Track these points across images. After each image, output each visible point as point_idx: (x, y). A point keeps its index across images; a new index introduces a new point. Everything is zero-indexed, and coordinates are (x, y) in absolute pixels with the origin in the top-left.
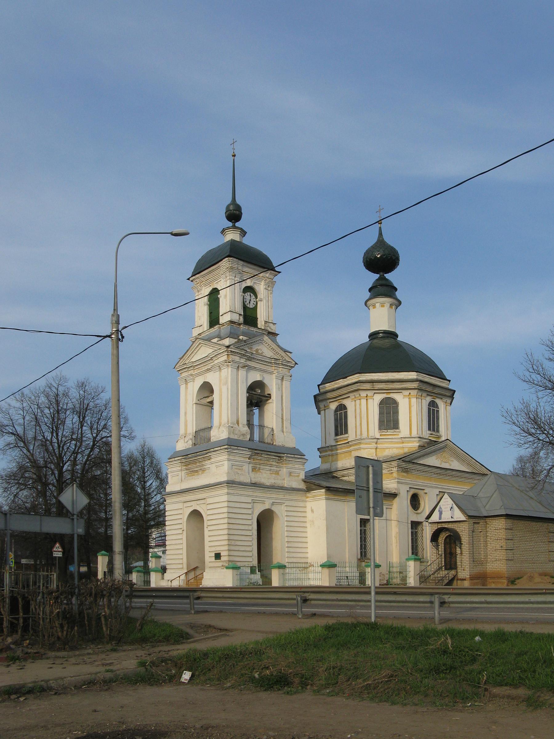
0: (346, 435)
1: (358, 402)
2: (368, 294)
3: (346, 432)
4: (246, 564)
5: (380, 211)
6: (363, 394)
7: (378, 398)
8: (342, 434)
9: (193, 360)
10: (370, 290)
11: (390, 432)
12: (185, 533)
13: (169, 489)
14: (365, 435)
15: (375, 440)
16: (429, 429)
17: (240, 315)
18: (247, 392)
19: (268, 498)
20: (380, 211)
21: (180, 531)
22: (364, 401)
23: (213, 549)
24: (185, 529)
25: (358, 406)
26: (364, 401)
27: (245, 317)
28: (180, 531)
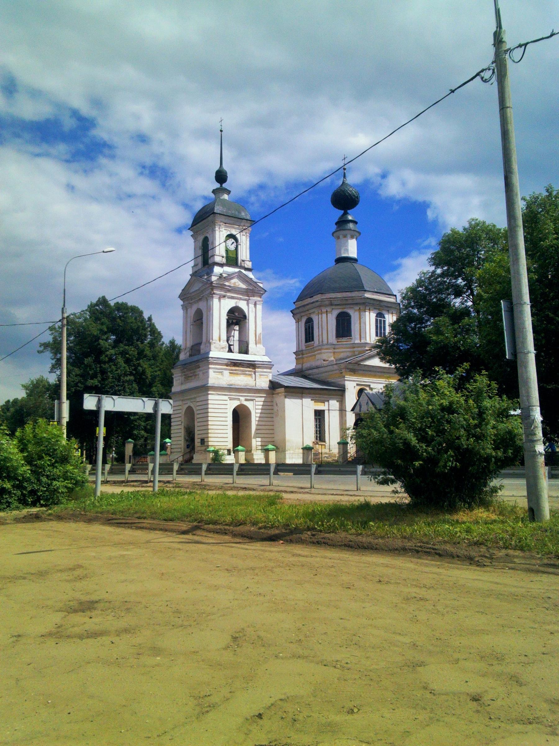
0: (313, 342)
1: (320, 316)
2: (334, 227)
3: (313, 340)
4: (223, 447)
5: (345, 159)
6: (324, 310)
7: (336, 313)
8: (310, 341)
9: (191, 291)
10: (336, 224)
11: (344, 339)
12: (183, 424)
13: (174, 389)
14: (325, 342)
15: (333, 346)
16: (377, 335)
17: (223, 257)
18: (227, 315)
19: (241, 396)
20: (345, 159)
21: (180, 423)
22: (324, 316)
23: (200, 436)
24: (183, 421)
25: (320, 319)
26: (324, 316)
27: (227, 258)
28: (180, 423)
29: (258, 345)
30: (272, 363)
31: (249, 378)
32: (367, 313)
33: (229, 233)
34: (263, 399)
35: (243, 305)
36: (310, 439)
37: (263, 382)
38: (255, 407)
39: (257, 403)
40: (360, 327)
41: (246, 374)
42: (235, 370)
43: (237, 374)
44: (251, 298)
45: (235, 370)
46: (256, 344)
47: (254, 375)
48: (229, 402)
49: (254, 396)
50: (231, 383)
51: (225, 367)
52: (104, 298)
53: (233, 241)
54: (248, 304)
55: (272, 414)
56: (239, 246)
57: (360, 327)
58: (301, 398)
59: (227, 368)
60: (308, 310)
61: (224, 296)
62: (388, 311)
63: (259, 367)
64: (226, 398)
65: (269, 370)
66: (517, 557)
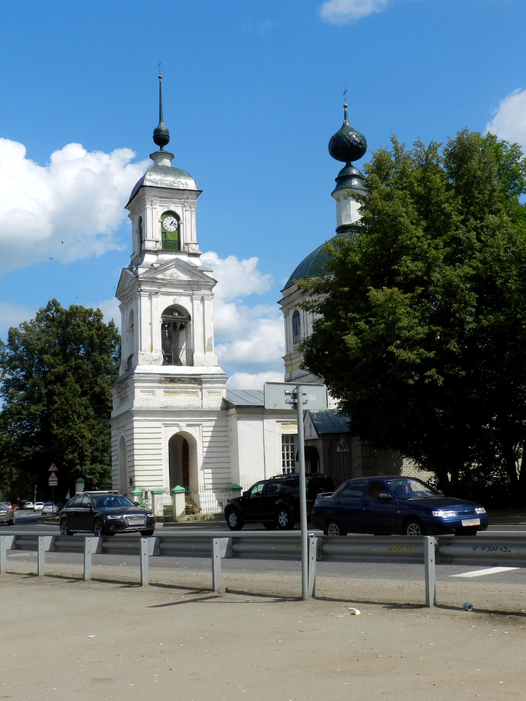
29: (207, 353)
31: (194, 397)
35: (184, 302)
38: (202, 436)
39: (205, 429)
41: (189, 392)
42: (173, 388)
43: (176, 392)
44: (195, 292)
45: (173, 388)
46: (205, 352)
48: (163, 429)
49: (199, 421)
50: (166, 405)
54: (192, 301)
56: (181, 226)
58: (262, 419)
63: (207, 382)
64: (159, 424)
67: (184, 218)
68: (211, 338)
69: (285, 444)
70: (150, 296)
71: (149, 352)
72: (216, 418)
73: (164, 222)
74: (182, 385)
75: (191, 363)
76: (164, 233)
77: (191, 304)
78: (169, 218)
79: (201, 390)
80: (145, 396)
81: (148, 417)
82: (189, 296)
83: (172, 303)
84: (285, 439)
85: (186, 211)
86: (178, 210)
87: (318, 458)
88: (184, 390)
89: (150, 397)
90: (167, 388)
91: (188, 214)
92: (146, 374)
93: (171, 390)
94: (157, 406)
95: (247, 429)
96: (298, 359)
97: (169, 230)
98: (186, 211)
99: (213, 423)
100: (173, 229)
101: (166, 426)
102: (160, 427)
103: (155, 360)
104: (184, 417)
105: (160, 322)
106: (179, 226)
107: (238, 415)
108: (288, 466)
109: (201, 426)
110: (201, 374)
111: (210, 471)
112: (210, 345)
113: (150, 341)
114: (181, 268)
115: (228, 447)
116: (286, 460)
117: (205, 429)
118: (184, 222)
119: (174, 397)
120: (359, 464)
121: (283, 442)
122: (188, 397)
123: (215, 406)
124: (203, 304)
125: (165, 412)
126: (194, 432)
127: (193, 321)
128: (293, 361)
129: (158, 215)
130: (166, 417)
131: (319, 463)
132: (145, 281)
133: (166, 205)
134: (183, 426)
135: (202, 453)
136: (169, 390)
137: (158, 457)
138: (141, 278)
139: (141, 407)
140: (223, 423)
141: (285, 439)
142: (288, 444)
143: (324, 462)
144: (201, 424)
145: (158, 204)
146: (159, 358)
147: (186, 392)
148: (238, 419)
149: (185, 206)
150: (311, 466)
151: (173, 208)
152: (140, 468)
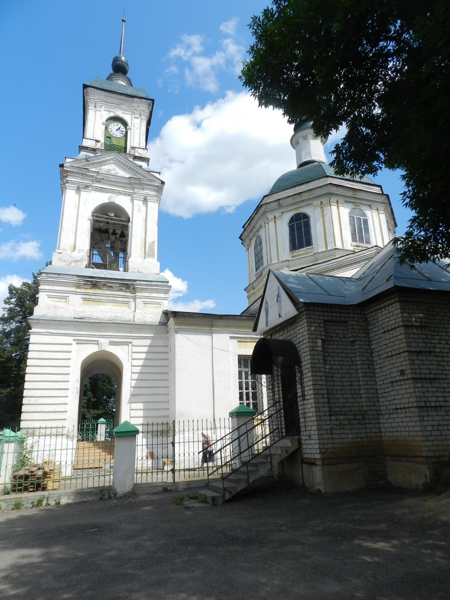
7: (287, 217)
11: (302, 251)
29: (146, 259)
30: (169, 284)
31: (124, 308)
32: (334, 208)
33: (112, 115)
34: (148, 342)
35: (123, 201)
36: (133, 344)
37: (151, 314)
38: (131, 359)
39: (135, 349)
40: (324, 229)
41: (118, 302)
42: (95, 295)
43: (99, 301)
44: (136, 191)
45: (95, 295)
46: (145, 258)
47: (132, 304)
48: (74, 347)
49: (128, 337)
50: (82, 315)
51: (74, 289)
52: (230, 413)
53: (120, 125)
54: (132, 201)
55: (160, 365)
56: (129, 132)
57: (324, 229)
58: (211, 333)
59: (78, 290)
60: (254, 227)
61: (87, 187)
62: (370, 206)
63: (142, 290)
64: (69, 340)
65: (163, 295)
66: (146, 181)
67: (133, 124)
68: (153, 242)
69: (243, 369)
70: (78, 190)
71: (69, 252)
72: (152, 335)
73: (110, 127)
74: (109, 292)
75: (126, 270)
76: (108, 137)
77: (131, 204)
78: (116, 124)
79: (135, 299)
80: (53, 303)
81: (54, 329)
82: (129, 195)
83: (106, 201)
84: (242, 362)
85: (135, 117)
86: (127, 118)
87: (298, 361)
88: (111, 298)
89: (61, 304)
90: (87, 294)
91: (137, 121)
92: (59, 274)
93: (93, 297)
94: (69, 316)
95: (188, 345)
96: (259, 287)
97: (115, 136)
98: (135, 117)
99: (148, 342)
100: (119, 134)
101: (79, 342)
102: (71, 344)
103: (75, 261)
104: (108, 331)
105: (89, 219)
106: (127, 133)
107: (177, 327)
108: (248, 399)
109: (130, 345)
110: (136, 281)
111: (141, 406)
112: (151, 250)
113: (74, 240)
114: (121, 165)
115: (167, 373)
116: (245, 391)
117: (135, 349)
118: (132, 128)
119: (96, 306)
120: (402, 372)
121: (240, 366)
122: (117, 307)
123: (151, 320)
124: (147, 207)
125: (80, 323)
126: (121, 353)
127: (132, 223)
128: (255, 290)
129: (102, 118)
130: (80, 330)
131: (301, 372)
132: (76, 173)
133: (113, 110)
134: (105, 345)
135: (130, 381)
136: (89, 297)
137: (62, 385)
138: (66, 167)
139: (44, 316)
140: (161, 343)
141: (242, 362)
142: (247, 369)
143: (314, 369)
144: (131, 342)
145: (103, 108)
146: (82, 259)
147: (113, 302)
148: (177, 332)
149: (134, 114)
150: (283, 383)
151: (120, 114)
152: (32, 400)
